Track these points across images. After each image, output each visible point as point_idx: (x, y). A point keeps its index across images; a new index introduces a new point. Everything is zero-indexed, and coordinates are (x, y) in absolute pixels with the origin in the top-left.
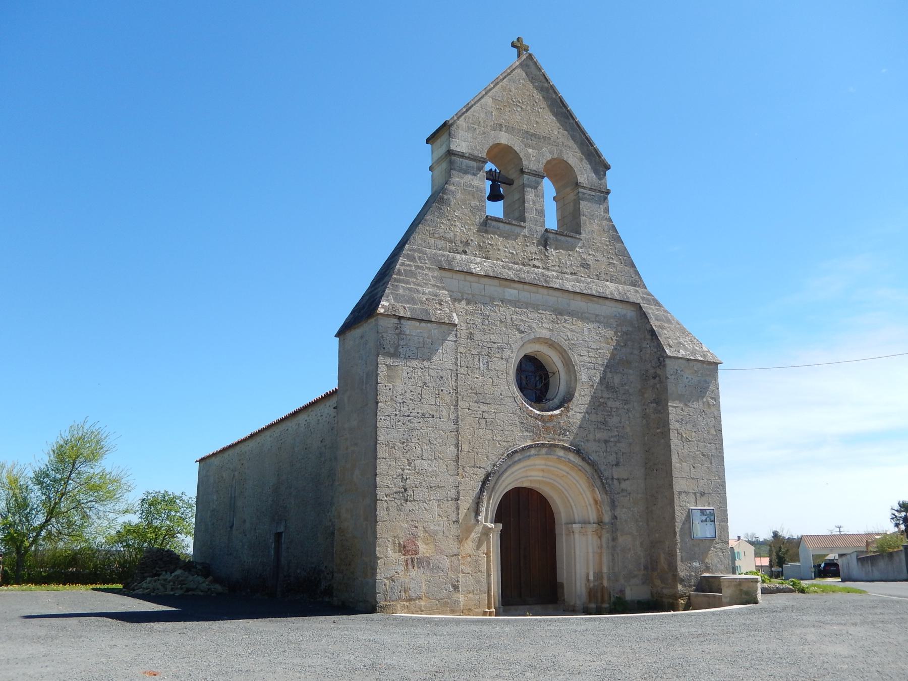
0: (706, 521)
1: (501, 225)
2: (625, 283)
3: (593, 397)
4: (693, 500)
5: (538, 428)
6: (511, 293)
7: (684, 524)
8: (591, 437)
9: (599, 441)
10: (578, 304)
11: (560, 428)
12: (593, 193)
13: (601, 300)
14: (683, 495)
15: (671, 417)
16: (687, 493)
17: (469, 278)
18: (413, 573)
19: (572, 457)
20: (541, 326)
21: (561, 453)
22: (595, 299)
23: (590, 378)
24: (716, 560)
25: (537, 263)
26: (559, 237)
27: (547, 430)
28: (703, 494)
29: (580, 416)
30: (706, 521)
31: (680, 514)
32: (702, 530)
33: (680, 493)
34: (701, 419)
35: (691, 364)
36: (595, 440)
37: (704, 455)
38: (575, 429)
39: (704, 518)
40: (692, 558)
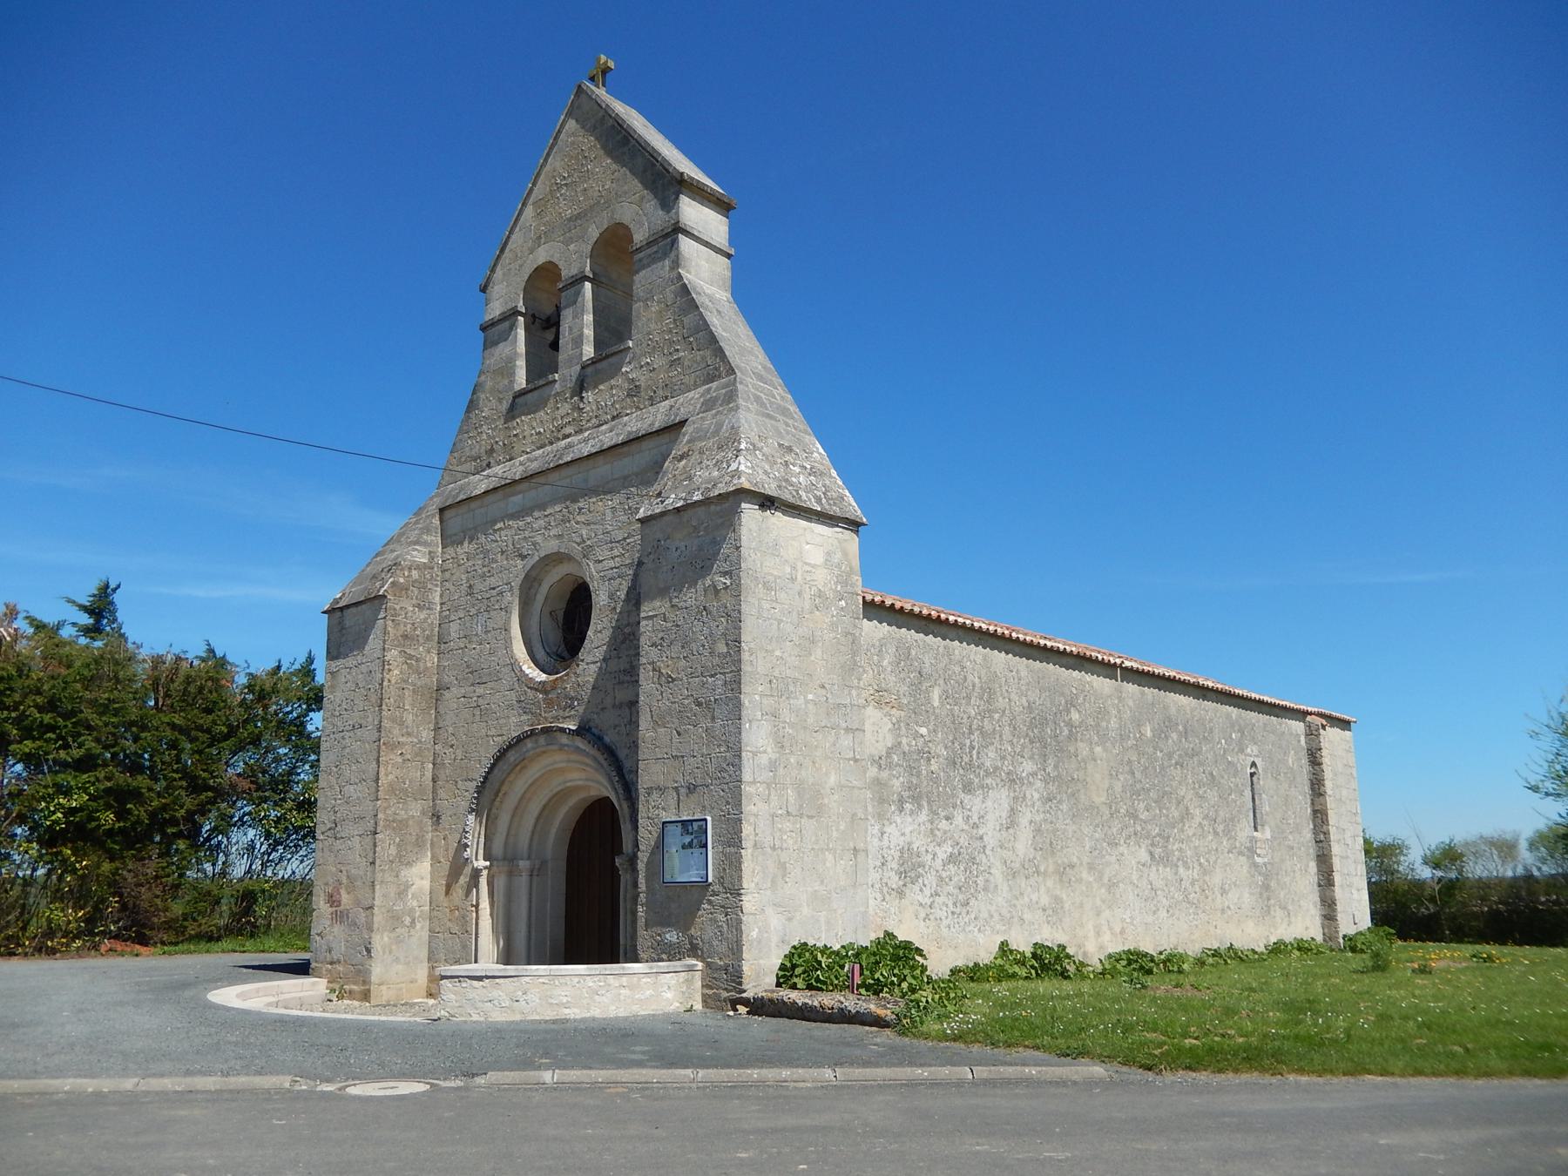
0: (690, 845)
1: (529, 396)
2: (696, 386)
3: (616, 629)
4: (672, 802)
5: (536, 704)
6: (517, 500)
7: (652, 853)
8: (609, 701)
9: (620, 706)
10: (603, 469)
11: (566, 697)
12: (655, 248)
13: (634, 447)
14: (655, 795)
15: (642, 640)
16: (662, 790)
17: (473, 505)
18: (337, 929)
19: (579, 742)
20: (544, 534)
21: (564, 739)
22: (625, 449)
23: (611, 596)
24: (710, 932)
25: (568, 430)
26: (599, 366)
27: (550, 704)
28: (691, 789)
29: (594, 668)
30: (690, 845)
31: (647, 835)
32: (682, 869)
33: (649, 791)
34: (698, 626)
35: (686, 516)
36: (614, 706)
37: (699, 704)
38: (586, 693)
39: (687, 839)
40: (666, 922)
